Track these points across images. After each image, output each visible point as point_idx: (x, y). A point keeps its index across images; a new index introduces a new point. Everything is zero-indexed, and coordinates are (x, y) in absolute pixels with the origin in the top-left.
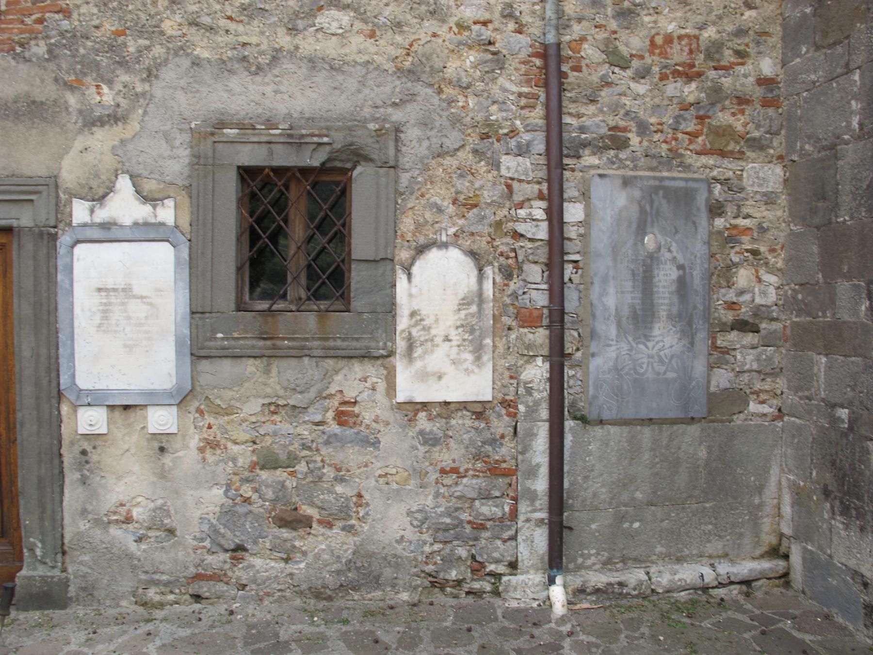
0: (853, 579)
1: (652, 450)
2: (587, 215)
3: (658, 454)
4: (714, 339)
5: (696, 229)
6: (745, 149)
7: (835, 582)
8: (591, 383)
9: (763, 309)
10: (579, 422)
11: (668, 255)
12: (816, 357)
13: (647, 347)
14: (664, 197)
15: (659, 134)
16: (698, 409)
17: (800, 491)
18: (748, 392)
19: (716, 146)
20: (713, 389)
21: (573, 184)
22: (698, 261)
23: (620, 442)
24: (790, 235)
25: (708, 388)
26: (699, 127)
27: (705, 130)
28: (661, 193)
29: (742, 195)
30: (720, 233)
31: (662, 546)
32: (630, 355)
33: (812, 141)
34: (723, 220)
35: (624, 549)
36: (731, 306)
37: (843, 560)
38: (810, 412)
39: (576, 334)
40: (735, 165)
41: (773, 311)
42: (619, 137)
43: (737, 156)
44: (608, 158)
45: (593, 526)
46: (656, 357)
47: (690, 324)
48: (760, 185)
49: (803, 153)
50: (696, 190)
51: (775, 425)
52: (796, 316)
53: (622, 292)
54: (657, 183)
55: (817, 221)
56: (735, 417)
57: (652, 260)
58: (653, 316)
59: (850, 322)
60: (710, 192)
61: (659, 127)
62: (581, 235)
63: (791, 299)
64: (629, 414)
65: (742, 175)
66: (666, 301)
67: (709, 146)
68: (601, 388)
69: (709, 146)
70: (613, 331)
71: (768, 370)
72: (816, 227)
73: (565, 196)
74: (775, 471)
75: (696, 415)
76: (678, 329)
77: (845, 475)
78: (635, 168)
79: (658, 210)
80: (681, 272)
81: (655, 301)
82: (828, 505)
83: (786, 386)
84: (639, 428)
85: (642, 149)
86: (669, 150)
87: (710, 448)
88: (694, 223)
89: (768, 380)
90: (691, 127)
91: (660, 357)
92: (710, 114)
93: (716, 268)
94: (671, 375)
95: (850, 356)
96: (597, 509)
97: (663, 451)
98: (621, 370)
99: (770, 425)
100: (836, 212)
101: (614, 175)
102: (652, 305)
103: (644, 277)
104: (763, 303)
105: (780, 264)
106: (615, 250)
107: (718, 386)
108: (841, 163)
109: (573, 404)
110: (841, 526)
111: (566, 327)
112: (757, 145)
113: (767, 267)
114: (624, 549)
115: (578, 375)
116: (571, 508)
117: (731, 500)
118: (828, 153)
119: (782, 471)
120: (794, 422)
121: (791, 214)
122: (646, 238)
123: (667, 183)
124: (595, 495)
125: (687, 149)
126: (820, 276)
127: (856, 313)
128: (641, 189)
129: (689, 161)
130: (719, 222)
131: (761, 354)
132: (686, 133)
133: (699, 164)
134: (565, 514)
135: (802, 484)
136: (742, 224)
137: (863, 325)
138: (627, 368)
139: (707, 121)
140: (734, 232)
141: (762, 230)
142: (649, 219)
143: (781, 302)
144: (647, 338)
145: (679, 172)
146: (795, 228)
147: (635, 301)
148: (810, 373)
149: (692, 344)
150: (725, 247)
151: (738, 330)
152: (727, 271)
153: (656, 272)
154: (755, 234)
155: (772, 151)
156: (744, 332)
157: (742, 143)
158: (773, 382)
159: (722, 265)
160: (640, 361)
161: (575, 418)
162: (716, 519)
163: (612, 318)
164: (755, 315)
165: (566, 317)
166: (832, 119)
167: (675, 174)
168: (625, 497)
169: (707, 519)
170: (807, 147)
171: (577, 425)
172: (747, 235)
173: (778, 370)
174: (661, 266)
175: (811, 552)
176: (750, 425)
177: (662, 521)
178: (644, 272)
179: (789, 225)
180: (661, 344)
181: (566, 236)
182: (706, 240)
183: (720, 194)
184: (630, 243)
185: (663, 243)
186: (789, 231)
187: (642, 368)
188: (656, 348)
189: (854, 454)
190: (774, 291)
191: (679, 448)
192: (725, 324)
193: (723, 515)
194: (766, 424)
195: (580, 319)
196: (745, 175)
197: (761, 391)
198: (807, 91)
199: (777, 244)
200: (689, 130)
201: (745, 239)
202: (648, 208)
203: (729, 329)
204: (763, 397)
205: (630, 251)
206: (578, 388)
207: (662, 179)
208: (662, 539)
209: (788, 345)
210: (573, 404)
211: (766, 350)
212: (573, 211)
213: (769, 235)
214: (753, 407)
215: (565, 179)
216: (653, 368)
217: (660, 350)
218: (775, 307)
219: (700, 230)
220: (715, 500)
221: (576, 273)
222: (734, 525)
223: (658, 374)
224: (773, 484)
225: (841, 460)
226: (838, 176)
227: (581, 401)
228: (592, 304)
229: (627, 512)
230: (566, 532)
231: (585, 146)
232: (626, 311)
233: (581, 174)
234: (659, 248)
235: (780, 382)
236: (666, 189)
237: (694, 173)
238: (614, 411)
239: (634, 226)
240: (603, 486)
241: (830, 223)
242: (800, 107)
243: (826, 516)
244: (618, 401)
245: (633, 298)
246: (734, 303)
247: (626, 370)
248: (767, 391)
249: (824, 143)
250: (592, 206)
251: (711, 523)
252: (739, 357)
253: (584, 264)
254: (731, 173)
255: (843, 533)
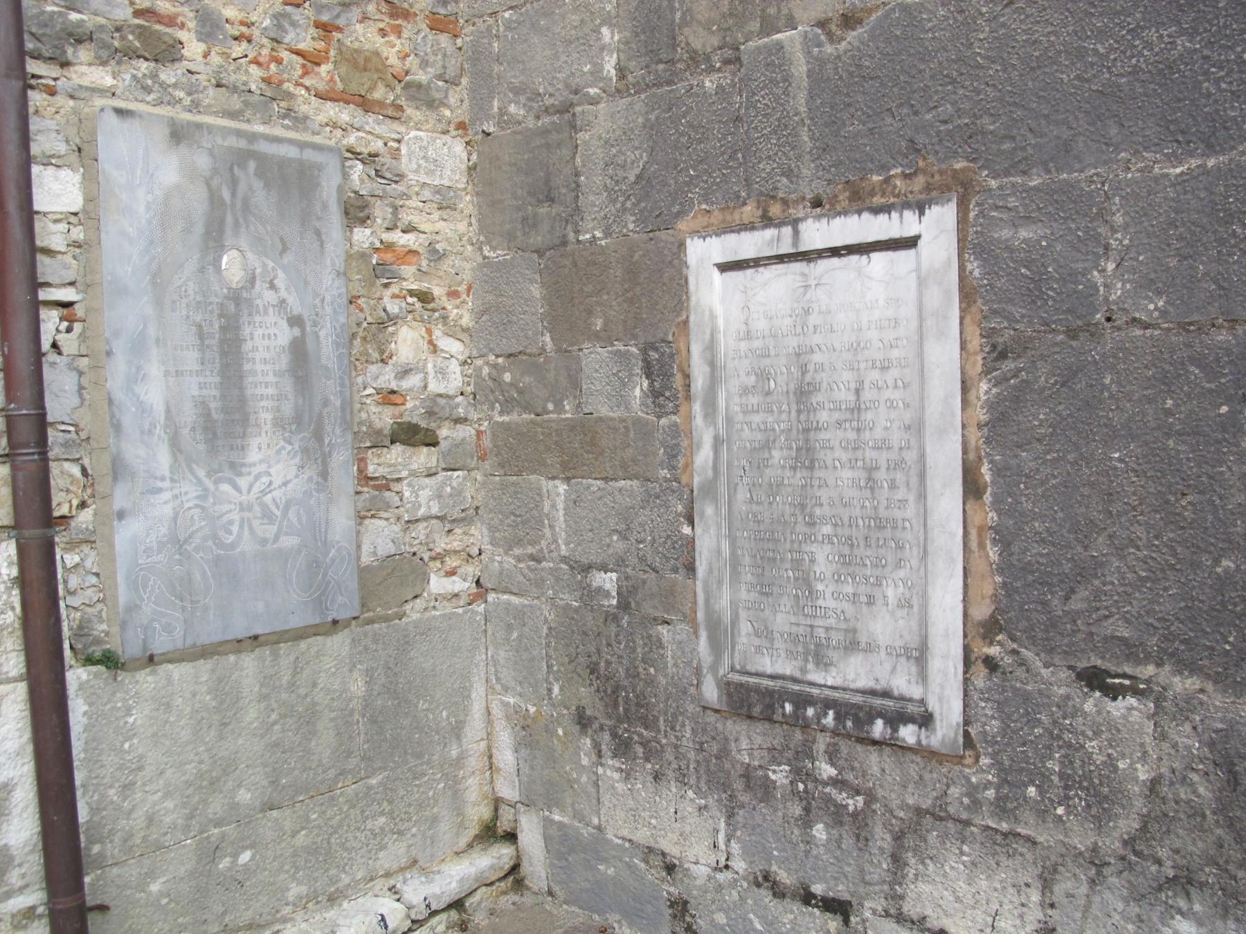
0: (647, 862)
1: (263, 698)
2: (90, 199)
3: (275, 705)
4: (362, 462)
5: (322, 246)
6: (402, 102)
7: (611, 871)
8: (120, 578)
9: (442, 401)
10: (101, 668)
11: (270, 296)
12: (546, 485)
13: (236, 488)
14: (260, 174)
15: (244, 44)
16: (344, 604)
17: (529, 721)
18: (426, 557)
19: (354, 88)
20: (366, 559)
21: (51, 124)
22: (328, 310)
23: (194, 695)
24: (482, 266)
25: (359, 558)
26: (321, 45)
27: (332, 53)
28: (252, 165)
29: (400, 188)
30: (363, 256)
31: (300, 883)
32: (203, 508)
33: (522, 99)
34: (368, 231)
35: (224, 913)
36: (389, 397)
37: (625, 833)
38: (539, 583)
39: (76, 470)
40: (388, 129)
41: (458, 405)
42: (159, 37)
43: (390, 112)
44: (134, 77)
45: (155, 887)
46: (257, 508)
47: (318, 435)
48: (430, 173)
49: (503, 119)
50: (320, 168)
51: (473, 611)
52: (501, 413)
53: (178, 374)
54: (243, 144)
55: (537, 240)
56: (408, 607)
57: (237, 305)
58: (245, 421)
59: (612, 419)
60: (346, 176)
61: (244, 29)
62: (76, 244)
63: (490, 383)
64: (210, 632)
65: (398, 149)
66: (270, 391)
67: (340, 86)
68: (145, 587)
69: (340, 86)
70: (163, 459)
71: (456, 514)
72: (537, 251)
73: (35, 149)
74: (478, 691)
75: (342, 615)
76: (297, 447)
77: (617, 689)
78: (195, 106)
79: (246, 201)
80: (296, 331)
81: (249, 392)
82: (588, 741)
83: (486, 539)
84: (232, 658)
85: (209, 69)
86: (264, 80)
87: (369, 673)
88: (318, 233)
89: (458, 531)
90: (307, 40)
91: (264, 506)
92: (341, 22)
93: (359, 325)
94: (288, 542)
95: (616, 480)
96: (159, 847)
97: (284, 696)
98: (186, 541)
99: (466, 613)
100: (576, 224)
101: (150, 114)
102: (242, 400)
103: (223, 341)
104: (442, 391)
105: (466, 321)
106: (158, 282)
107: (375, 553)
108: (582, 136)
109: (81, 631)
110: (616, 776)
111: (51, 455)
112: (421, 95)
113: (445, 324)
114: (224, 913)
115: (88, 564)
116: (100, 862)
117: (413, 762)
118: (556, 118)
119: (490, 689)
120: (509, 603)
121: (484, 227)
122: (225, 259)
123: (263, 147)
124: (151, 820)
125: (297, 84)
126: (548, 339)
127: (623, 402)
128: (211, 152)
129: (304, 109)
130: (362, 236)
131: (444, 484)
132: (298, 53)
133: (322, 118)
134: (87, 879)
135: (532, 710)
136: (402, 242)
137: (638, 421)
138: (199, 534)
139: (336, 35)
140: (389, 257)
141: (437, 256)
142: (229, 219)
143: (469, 389)
144: (236, 468)
145: (287, 127)
146: (492, 254)
147: (205, 392)
148: (535, 512)
149: (324, 474)
150: (373, 284)
151: (404, 443)
152: (380, 330)
153: (246, 331)
154: (424, 263)
155: (447, 113)
156: (414, 445)
157: (398, 89)
158: (465, 533)
159: (370, 319)
160: (225, 519)
161: (89, 661)
162: (390, 802)
163: (158, 430)
164: (430, 413)
165: (50, 432)
166: (563, 58)
167: (278, 132)
168: (216, 806)
169: (375, 807)
170: (512, 109)
171: (96, 675)
172: (409, 264)
173: (472, 512)
174: (258, 319)
175: (561, 825)
176: (434, 617)
177: (295, 834)
178: (224, 329)
179: (481, 249)
180: (265, 479)
181: (39, 243)
182: (342, 270)
183: (362, 182)
184: (191, 266)
185: (258, 271)
186: (480, 259)
187: (230, 533)
188: (256, 489)
189: (634, 650)
190: (458, 369)
191: (314, 685)
192: (379, 432)
193: (402, 792)
194: (460, 611)
195: (83, 435)
196: (404, 151)
197: (447, 552)
198: (511, 8)
199: (460, 284)
200: (301, 46)
201: (408, 270)
202: (226, 194)
203: (388, 443)
204: (451, 562)
205: (190, 284)
206: (89, 592)
207: (253, 137)
208: (297, 869)
209: (487, 465)
210: (81, 631)
211: (451, 477)
212: (56, 187)
213: (447, 265)
214: (438, 584)
215: (31, 110)
216: (251, 529)
217: (264, 493)
218: (460, 398)
219: (329, 247)
220: (384, 768)
221: (69, 330)
222: (420, 807)
223: (264, 541)
224: (477, 716)
225: (608, 663)
226: (578, 160)
227: (102, 622)
228: (110, 402)
229: (223, 837)
230: (93, 919)
231: (79, 41)
232: (188, 415)
233: (71, 103)
234: (252, 280)
235: (476, 533)
236: (261, 158)
237: (314, 133)
238: (179, 632)
239: (199, 229)
240: (167, 795)
241: (564, 243)
242: (497, 36)
243: (585, 761)
244: (184, 608)
245: (201, 386)
246: (393, 392)
247: (197, 541)
248: (455, 552)
249: (549, 101)
250: (101, 178)
251: (382, 813)
252: (407, 494)
253: (88, 311)
254: (380, 143)
255: (620, 787)
